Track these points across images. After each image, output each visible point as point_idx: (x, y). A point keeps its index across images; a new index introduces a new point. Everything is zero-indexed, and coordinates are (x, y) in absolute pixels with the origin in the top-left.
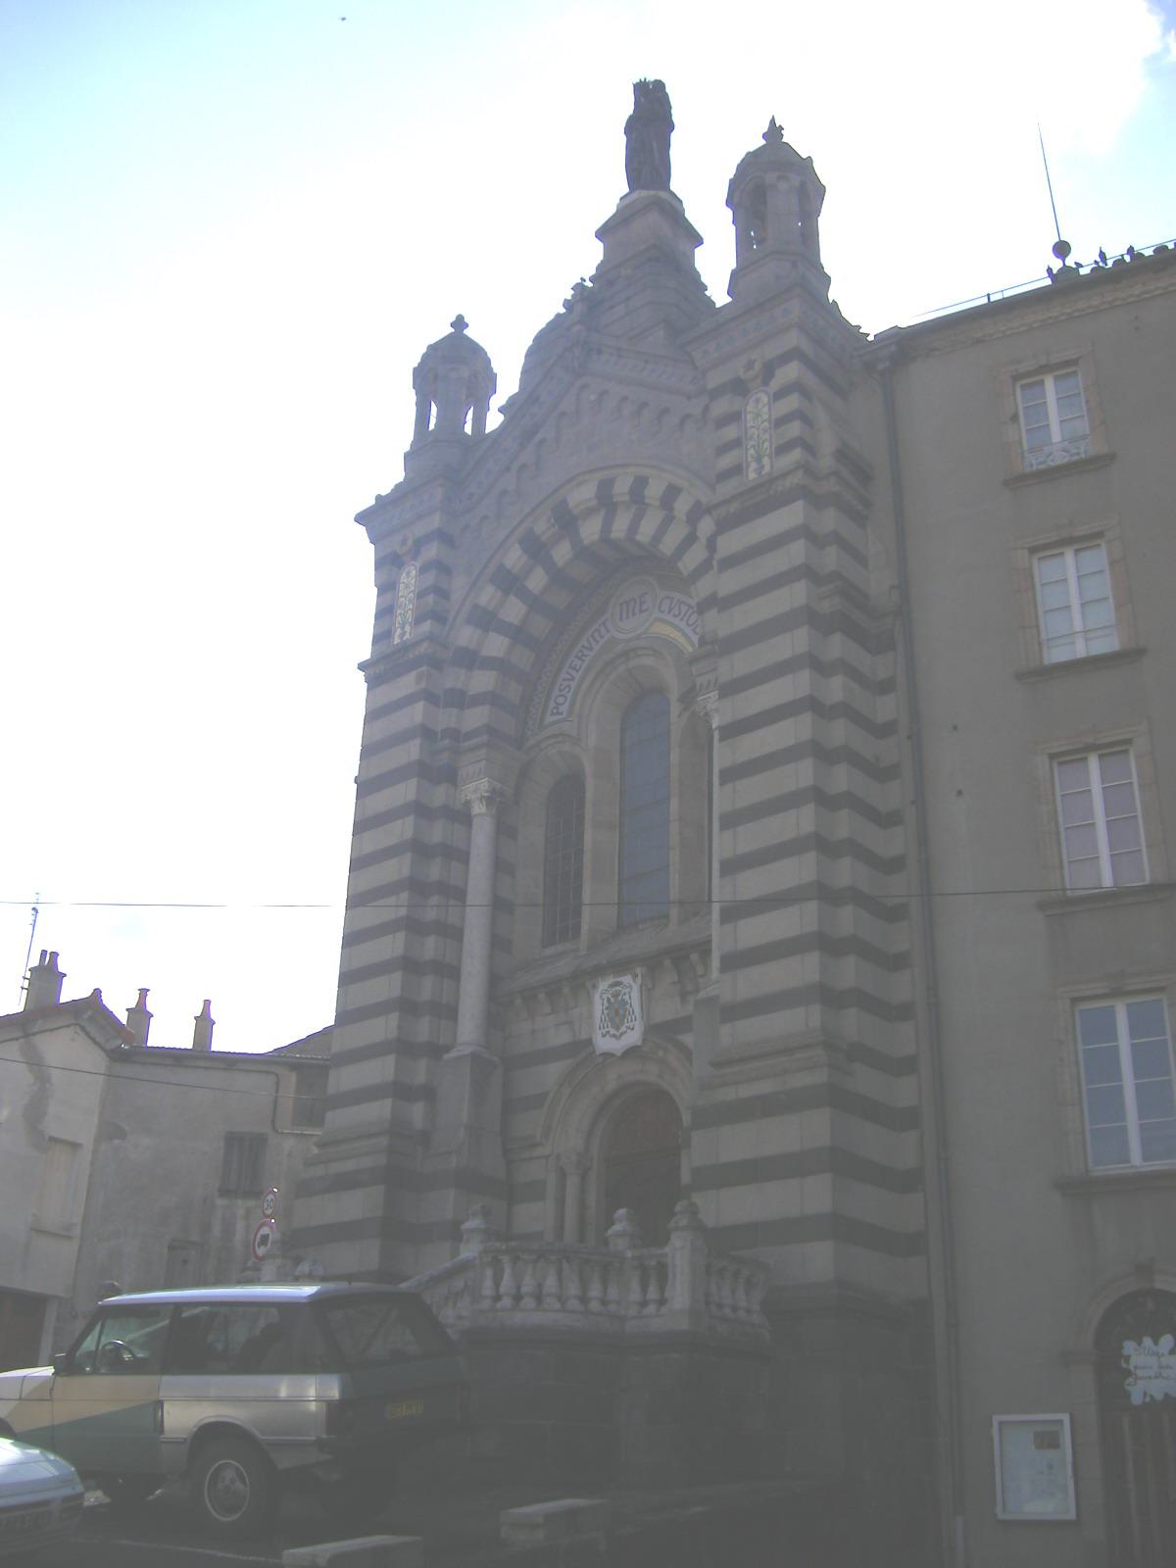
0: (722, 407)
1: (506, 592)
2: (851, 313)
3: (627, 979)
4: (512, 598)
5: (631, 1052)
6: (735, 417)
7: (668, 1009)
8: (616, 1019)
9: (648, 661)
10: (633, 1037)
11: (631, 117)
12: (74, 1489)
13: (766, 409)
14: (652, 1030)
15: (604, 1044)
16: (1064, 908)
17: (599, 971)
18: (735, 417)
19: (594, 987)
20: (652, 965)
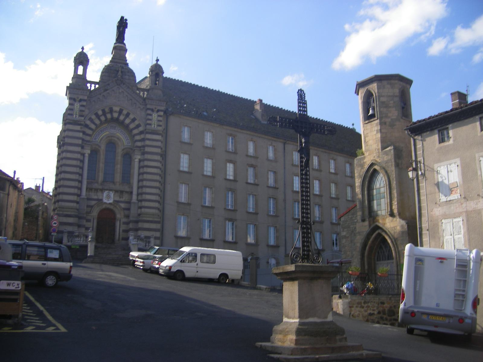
0: (149, 112)
1: (119, 112)
2: (87, 79)
3: (111, 192)
4: (130, 121)
5: (110, 204)
6: (151, 115)
7: (117, 199)
8: (108, 198)
9: (116, 139)
10: (111, 201)
11: (242, 98)
12: (379, 299)
13: (153, 118)
14: (115, 201)
15: (105, 201)
16: (179, 203)
17: (107, 190)
18: (151, 115)
19: (105, 192)
20: (116, 191)
